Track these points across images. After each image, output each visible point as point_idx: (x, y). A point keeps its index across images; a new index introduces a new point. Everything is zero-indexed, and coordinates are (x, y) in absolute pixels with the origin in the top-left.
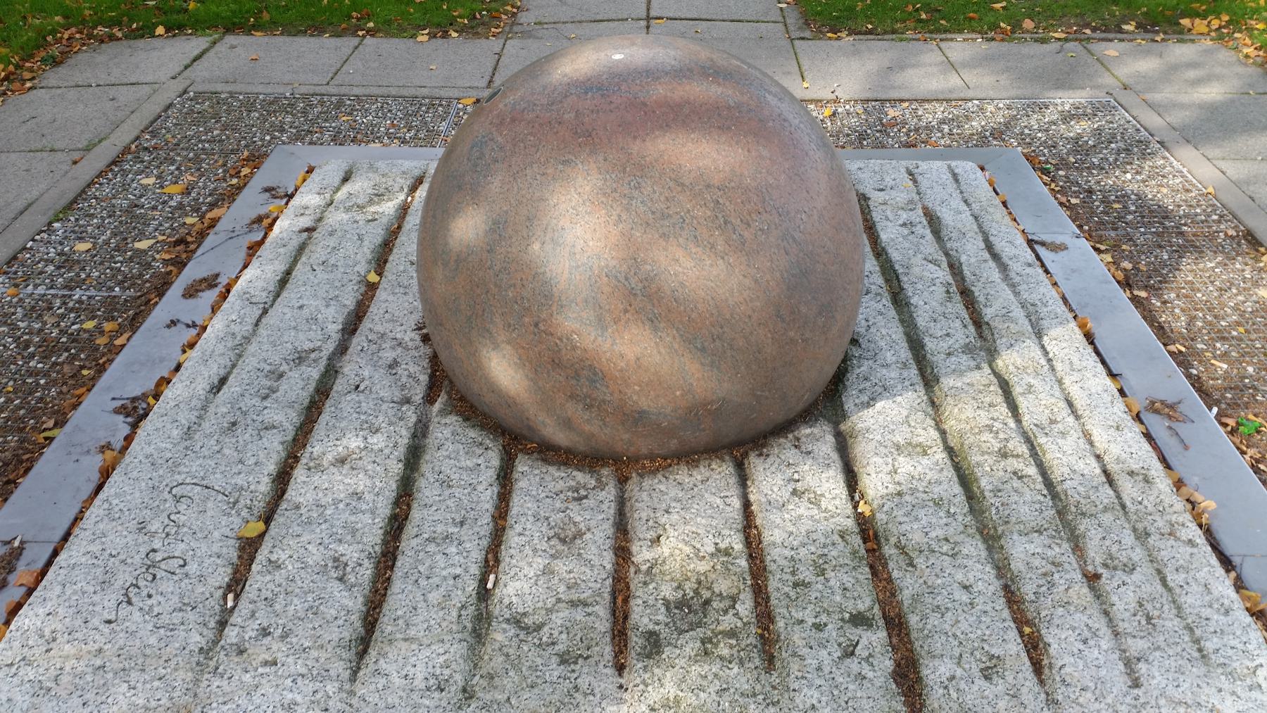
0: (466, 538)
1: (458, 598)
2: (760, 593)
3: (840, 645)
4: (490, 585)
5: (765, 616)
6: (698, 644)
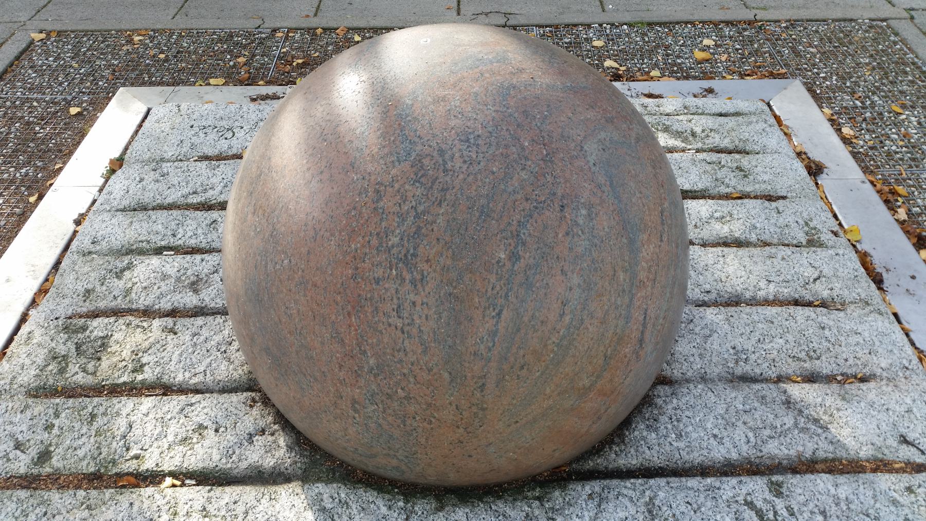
0: (757, 416)
1: (153, 238)
2: (97, 390)
3: (29, 440)
4: (165, 253)
5: (70, 392)
6: (63, 353)
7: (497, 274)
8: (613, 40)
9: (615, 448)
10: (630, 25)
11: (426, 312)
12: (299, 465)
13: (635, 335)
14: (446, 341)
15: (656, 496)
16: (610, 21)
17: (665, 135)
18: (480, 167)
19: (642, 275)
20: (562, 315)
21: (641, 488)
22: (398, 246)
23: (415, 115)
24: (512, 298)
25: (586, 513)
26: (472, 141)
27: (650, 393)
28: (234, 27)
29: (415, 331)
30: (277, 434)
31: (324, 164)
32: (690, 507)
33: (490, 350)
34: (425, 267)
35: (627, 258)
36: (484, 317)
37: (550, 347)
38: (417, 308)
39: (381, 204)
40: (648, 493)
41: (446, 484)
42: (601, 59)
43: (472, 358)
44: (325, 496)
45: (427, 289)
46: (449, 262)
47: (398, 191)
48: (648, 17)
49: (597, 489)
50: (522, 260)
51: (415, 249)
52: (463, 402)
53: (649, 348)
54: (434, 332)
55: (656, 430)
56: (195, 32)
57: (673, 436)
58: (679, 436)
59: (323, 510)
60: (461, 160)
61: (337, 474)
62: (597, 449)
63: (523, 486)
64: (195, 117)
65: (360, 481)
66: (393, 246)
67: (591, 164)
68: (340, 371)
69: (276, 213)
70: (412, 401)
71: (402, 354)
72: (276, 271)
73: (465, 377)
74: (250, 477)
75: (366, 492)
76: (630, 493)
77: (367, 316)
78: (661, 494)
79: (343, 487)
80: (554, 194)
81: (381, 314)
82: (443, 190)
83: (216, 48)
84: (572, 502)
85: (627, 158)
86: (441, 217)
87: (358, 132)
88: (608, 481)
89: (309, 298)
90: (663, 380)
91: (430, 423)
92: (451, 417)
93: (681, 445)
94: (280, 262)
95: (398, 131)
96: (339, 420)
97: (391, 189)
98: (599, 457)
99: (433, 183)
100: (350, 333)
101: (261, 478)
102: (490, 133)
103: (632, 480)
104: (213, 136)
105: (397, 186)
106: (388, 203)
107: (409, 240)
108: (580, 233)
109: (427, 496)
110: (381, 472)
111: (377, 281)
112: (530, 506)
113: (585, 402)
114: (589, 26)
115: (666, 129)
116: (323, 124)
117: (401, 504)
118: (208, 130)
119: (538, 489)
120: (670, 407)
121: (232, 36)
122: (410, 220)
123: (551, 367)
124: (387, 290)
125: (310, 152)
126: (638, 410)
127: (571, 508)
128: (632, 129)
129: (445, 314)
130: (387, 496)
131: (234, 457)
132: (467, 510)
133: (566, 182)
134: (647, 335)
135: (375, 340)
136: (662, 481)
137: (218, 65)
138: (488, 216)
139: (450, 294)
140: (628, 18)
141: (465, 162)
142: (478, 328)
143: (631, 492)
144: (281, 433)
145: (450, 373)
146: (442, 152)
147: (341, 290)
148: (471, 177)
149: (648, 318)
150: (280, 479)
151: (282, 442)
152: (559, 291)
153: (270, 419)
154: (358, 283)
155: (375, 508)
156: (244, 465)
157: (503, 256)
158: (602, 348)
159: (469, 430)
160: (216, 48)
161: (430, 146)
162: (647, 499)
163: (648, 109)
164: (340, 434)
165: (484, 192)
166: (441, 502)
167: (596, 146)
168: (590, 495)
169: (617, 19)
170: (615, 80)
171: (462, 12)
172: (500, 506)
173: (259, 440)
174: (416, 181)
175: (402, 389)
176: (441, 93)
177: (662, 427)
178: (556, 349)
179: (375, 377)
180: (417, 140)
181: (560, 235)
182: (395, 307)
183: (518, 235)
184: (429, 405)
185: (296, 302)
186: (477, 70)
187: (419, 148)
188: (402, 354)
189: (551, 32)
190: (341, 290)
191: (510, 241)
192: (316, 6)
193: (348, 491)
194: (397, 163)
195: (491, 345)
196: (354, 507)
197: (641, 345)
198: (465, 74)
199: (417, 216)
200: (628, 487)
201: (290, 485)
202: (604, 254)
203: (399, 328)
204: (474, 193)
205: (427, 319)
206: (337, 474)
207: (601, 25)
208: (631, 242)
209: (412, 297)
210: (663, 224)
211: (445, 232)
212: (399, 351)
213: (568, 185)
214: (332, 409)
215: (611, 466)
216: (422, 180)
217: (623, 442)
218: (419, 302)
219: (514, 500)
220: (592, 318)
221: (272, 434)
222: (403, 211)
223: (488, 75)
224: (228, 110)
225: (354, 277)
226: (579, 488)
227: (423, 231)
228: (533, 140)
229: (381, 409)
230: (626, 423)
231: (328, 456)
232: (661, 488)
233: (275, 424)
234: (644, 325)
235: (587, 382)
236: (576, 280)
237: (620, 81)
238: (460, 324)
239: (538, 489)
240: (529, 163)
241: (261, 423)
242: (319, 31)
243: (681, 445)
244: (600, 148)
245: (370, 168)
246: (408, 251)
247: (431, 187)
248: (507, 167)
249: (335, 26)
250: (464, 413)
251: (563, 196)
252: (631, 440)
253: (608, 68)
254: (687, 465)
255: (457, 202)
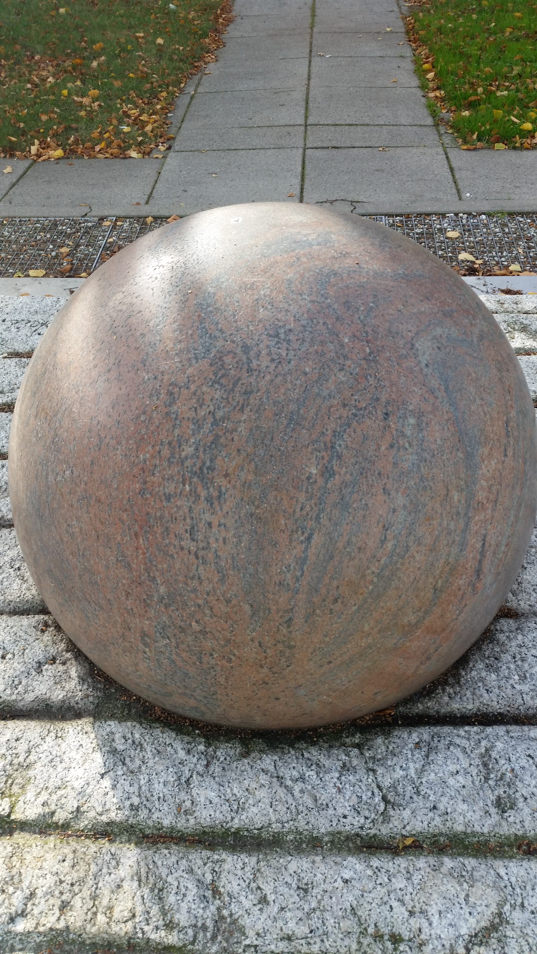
7: (307, 492)
8: (469, 230)
9: (449, 690)
10: (489, 215)
11: (223, 534)
12: (91, 699)
13: (471, 565)
14: (246, 569)
15: (493, 747)
16: (467, 210)
17: (522, 335)
18: (290, 366)
19: (481, 496)
20: (383, 541)
21: (477, 737)
22: (192, 457)
23: (218, 305)
24: (324, 520)
25: (411, 765)
26: (282, 336)
27: (492, 627)
28: (60, 215)
29: (211, 556)
30: (68, 663)
31: (112, 360)
32: (531, 761)
33: (298, 580)
34: (223, 482)
35: (462, 476)
36: (291, 541)
37: (369, 578)
38: (213, 530)
39: (175, 408)
40: (484, 743)
41: (253, 727)
42: (455, 251)
43: (277, 588)
44: (117, 736)
45: (225, 509)
46: (251, 477)
47: (194, 394)
48: (509, 206)
49: (426, 737)
50: (337, 477)
51: (211, 461)
52: (267, 638)
53: (488, 579)
54: (233, 558)
55: (497, 670)
56: (18, 220)
57: (516, 677)
58: (523, 678)
59: (114, 752)
60: (269, 359)
61: (133, 711)
62: (428, 691)
63: (341, 732)
64: (8, 310)
65: (158, 720)
66: (186, 458)
67: (423, 365)
68: (127, 599)
69: (59, 416)
70: (209, 636)
71: (196, 583)
72: (57, 483)
73: (269, 609)
74: (37, 711)
75: (163, 732)
76: (464, 743)
77: (156, 538)
78: (499, 745)
79: (138, 726)
80: (378, 400)
81: (172, 536)
82: (245, 393)
83: (38, 238)
84: (397, 751)
85: (468, 358)
86: (242, 424)
87: (151, 324)
88: (439, 728)
89: (92, 515)
90: (507, 613)
91: (230, 661)
92: (254, 655)
93: (525, 688)
94: (62, 473)
95: (197, 324)
96: (128, 654)
97: (186, 391)
98: (430, 700)
99: (235, 385)
100: (137, 557)
101: (48, 712)
102: (304, 326)
103: (467, 728)
104: (25, 330)
105: (193, 387)
106: (182, 407)
107: (205, 450)
108: (407, 445)
109: (231, 739)
110: (180, 711)
111: (168, 498)
112: (347, 755)
113: (410, 641)
114: (444, 215)
115: (524, 329)
116: (114, 315)
117: (202, 748)
118: (21, 325)
119: (358, 735)
120: (514, 644)
121: (56, 225)
122: (207, 426)
123: (369, 600)
124: (179, 508)
125: (97, 348)
126: (477, 646)
127: (395, 759)
128: (475, 325)
129: (246, 537)
130: (186, 739)
131: (20, 688)
132: (276, 758)
133: (392, 385)
134: (487, 565)
135: (165, 566)
136: (501, 730)
137: (40, 255)
138: (298, 424)
139: (252, 515)
140: (487, 207)
141: (273, 360)
142: (283, 554)
143: (464, 741)
144: (73, 662)
145: (252, 606)
146: (246, 349)
147: (128, 507)
148: (280, 378)
149: (487, 545)
150: (70, 714)
151: (73, 673)
152: (380, 512)
153: (62, 646)
154: (147, 499)
155: (172, 752)
156: (30, 697)
157: (315, 472)
158: (431, 580)
159: (274, 670)
160: (38, 238)
161: (233, 342)
162: (483, 750)
163: (505, 306)
164: (130, 668)
165: (294, 395)
166: (247, 746)
167: (430, 344)
168: (417, 743)
169: (474, 208)
170: (470, 275)
171: (305, 199)
172: (314, 753)
173: (49, 670)
174: (215, 382)
175: (197, 622)
176: (249, 279)
177: (504, 667)
178: (375, 580)
179: (166, 608)
180: (218, 334)
181: (383, 448)
182: (189, 528)
183: (332, 447)
184: (228, 641)
185: (78, 519)
186: (292, 254)
187: (220, 343)
188: (196, 583)
189: (401, 221)
190: (128, 507)
191: (324, 453)
192: (148, 193)
193: (143, 730)
194: (194, 361)
195: (299, 574)
196: (149, 749)
197: (478, 575)
198: (279, 258)
199: (215, 423)
200: (462, 735)
201: (80, 722)
202: (435, 470)
203: (193, 553)
204: (282, 397)
205: (224, 543)
206: (133, 711)
207: (456, 215)
208: (469, 456)
209: (207, 517)
210: (508, 436)
211: (247, 442)
212: (192, 578)
213: (394, 389)
214: (120, 641)
215: (443, 711)
216: (223, 381)
217: (458, 683)
218: (215, 523)
219: (331, 747)
220: (419, 544)
221: (64, 664)
222: (199, 417)
223: (304, 260)
224: (43, 304)
225: (142, 492)
226: (405, 735)
227: (222, 440)
228: (354, 336)
229: (174, 644)
230: (463, 662)
231: (124, 690)
232: (499, 738)
233: (67, 651)
234: (483, 553)
235: (412, 618)
236: (400, 500)
237: (475, 275)
238: (262, 549)
239: (358, 735)
240: (349, 363)
241: (52, 651)
242: (149, 220)
243: (525, 688)
244: (435, 346)
245: (164, 366)
246: (204, 464)
247: (233, 390)
248: (322, 367)
249: (167, 214)
250: (268, 651)
251: (388, 402)
252: (467, 681)
253: (463, 261)
254: (531, 712)
255: (262, 408)
